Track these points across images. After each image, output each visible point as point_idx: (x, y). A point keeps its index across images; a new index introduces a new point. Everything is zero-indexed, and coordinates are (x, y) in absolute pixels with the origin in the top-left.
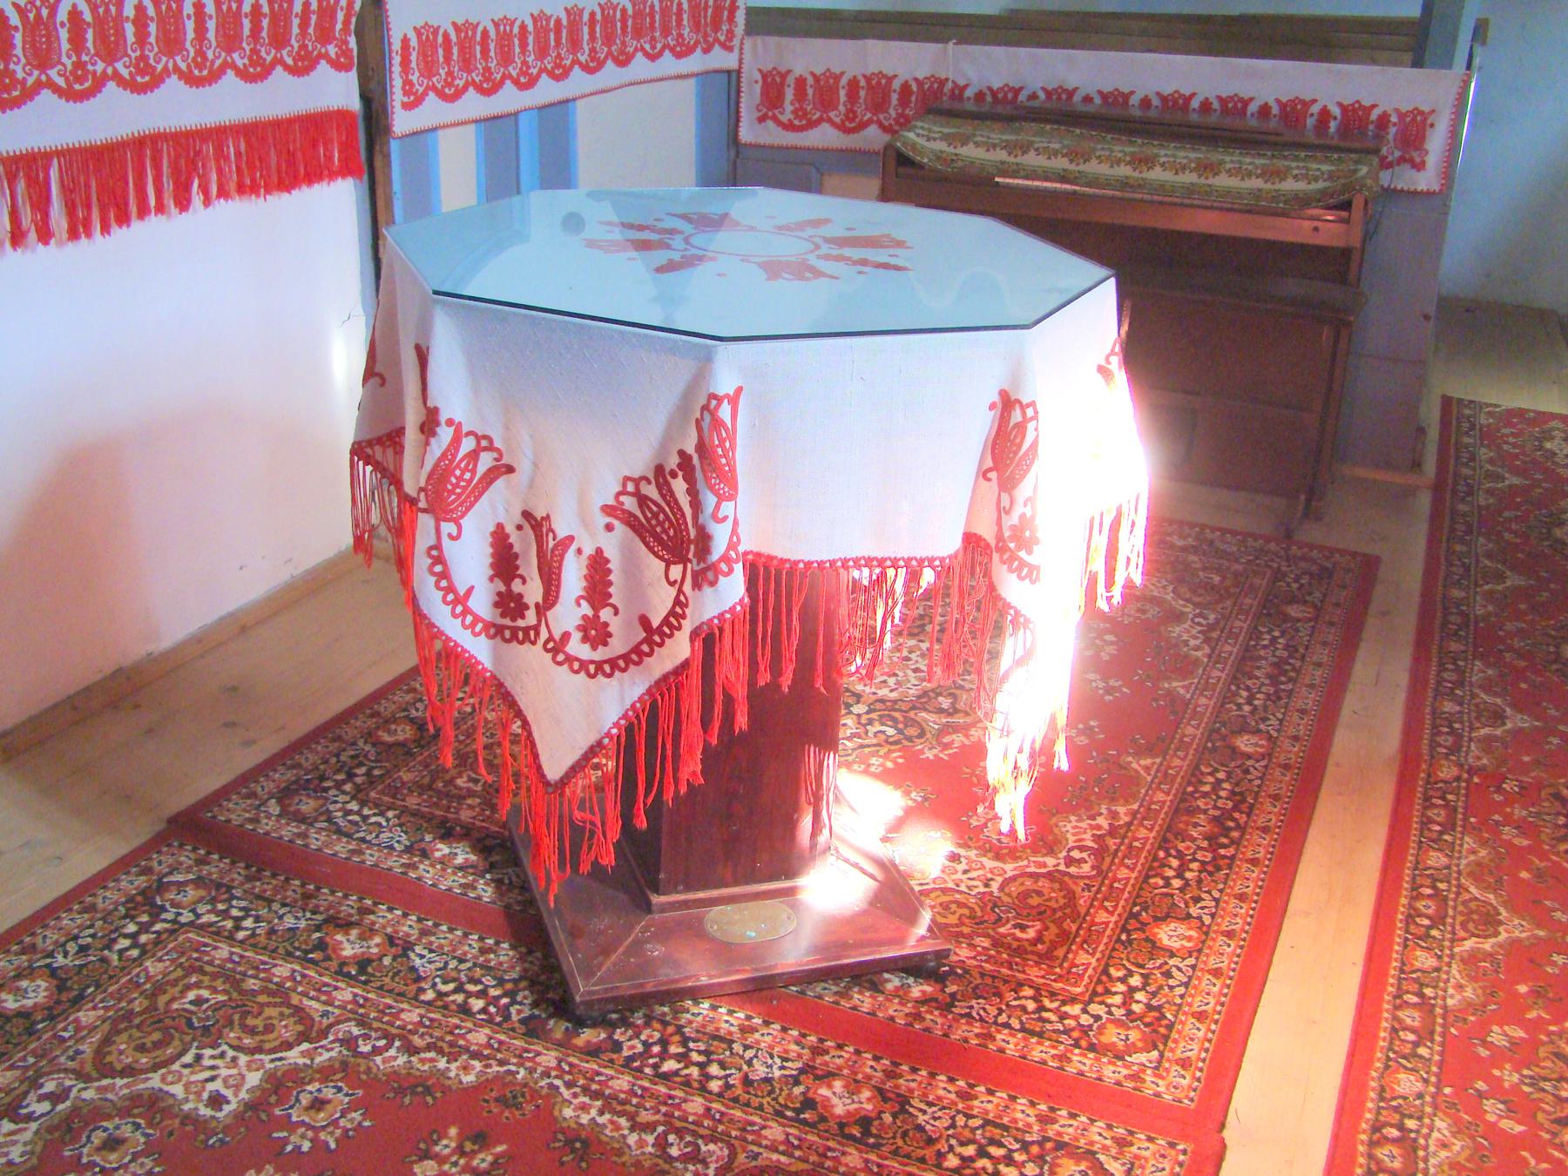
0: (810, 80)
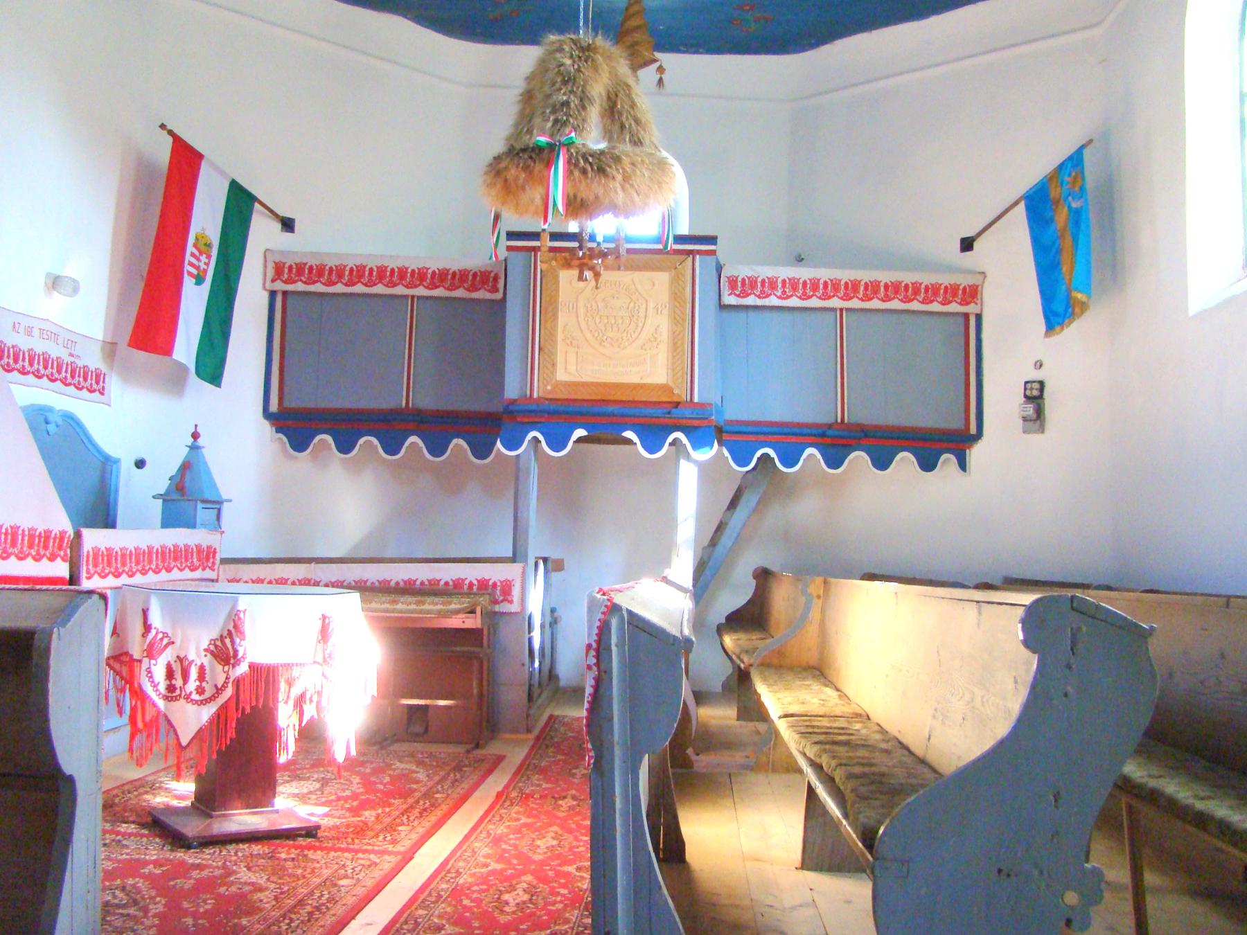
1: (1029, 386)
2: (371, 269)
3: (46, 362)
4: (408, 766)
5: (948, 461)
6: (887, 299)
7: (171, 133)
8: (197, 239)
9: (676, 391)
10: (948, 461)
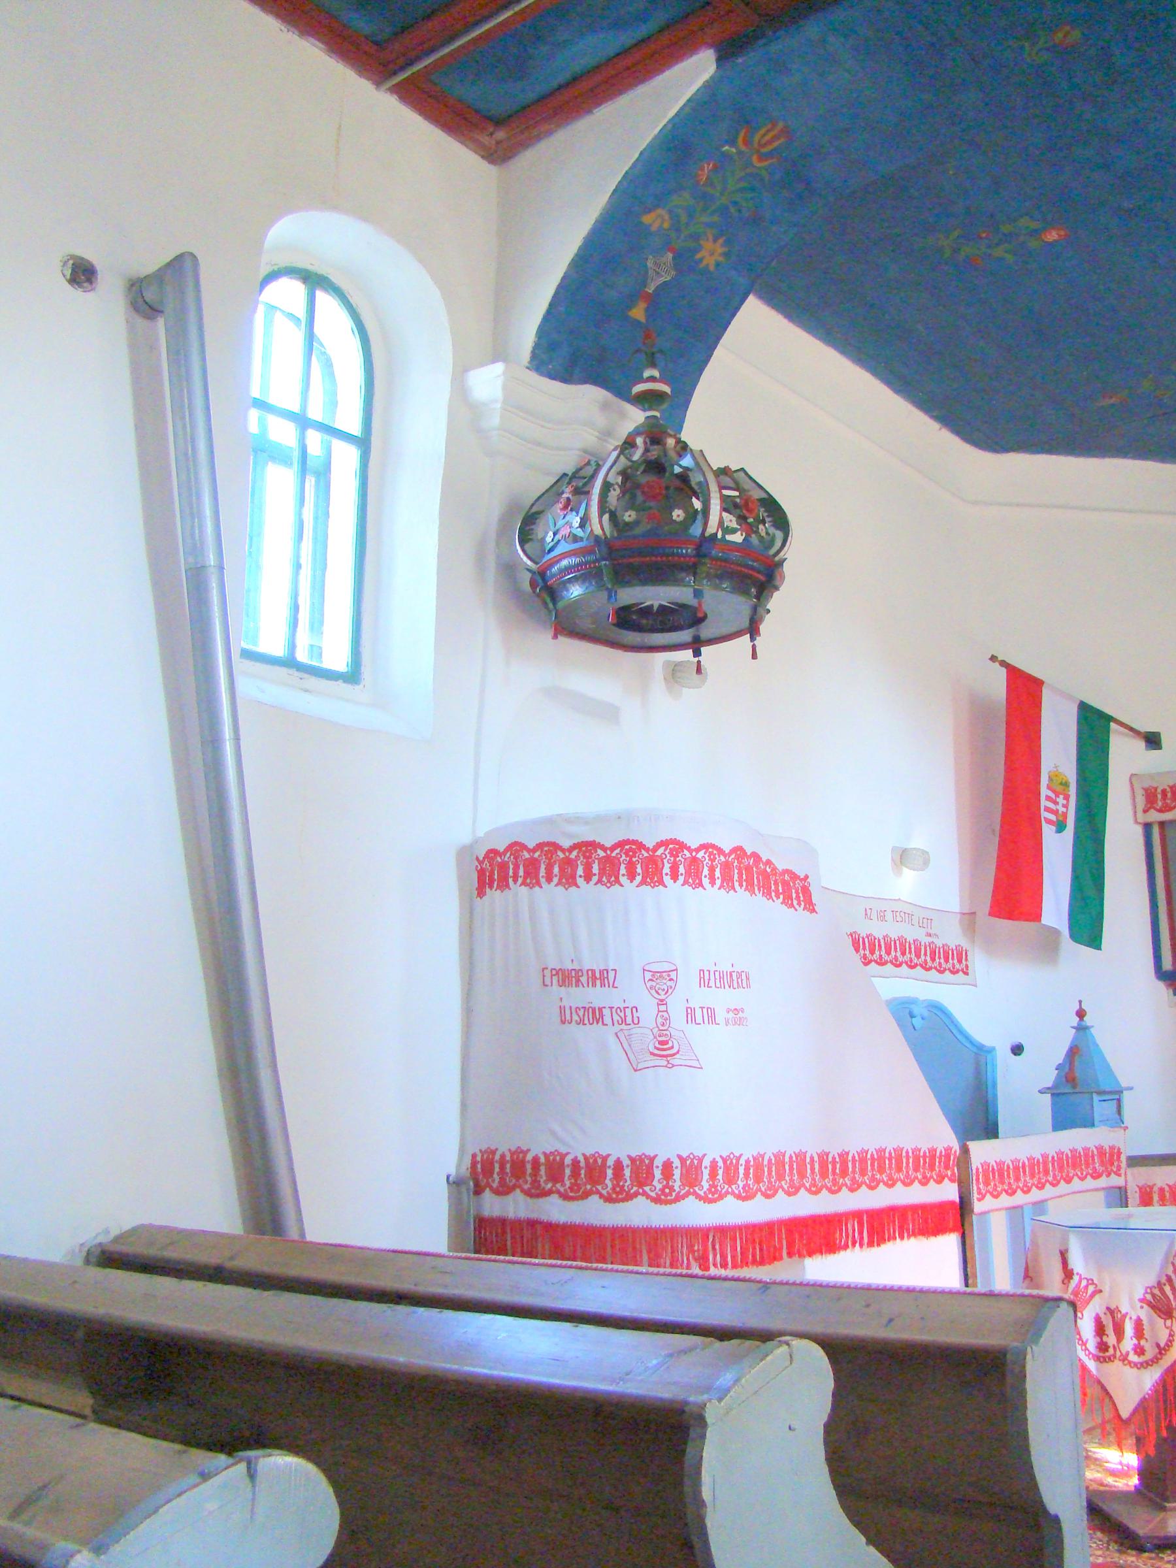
0: (1167, 1189)
3: (903, 946)
7: (1003, 663)
8: (1050, 779)
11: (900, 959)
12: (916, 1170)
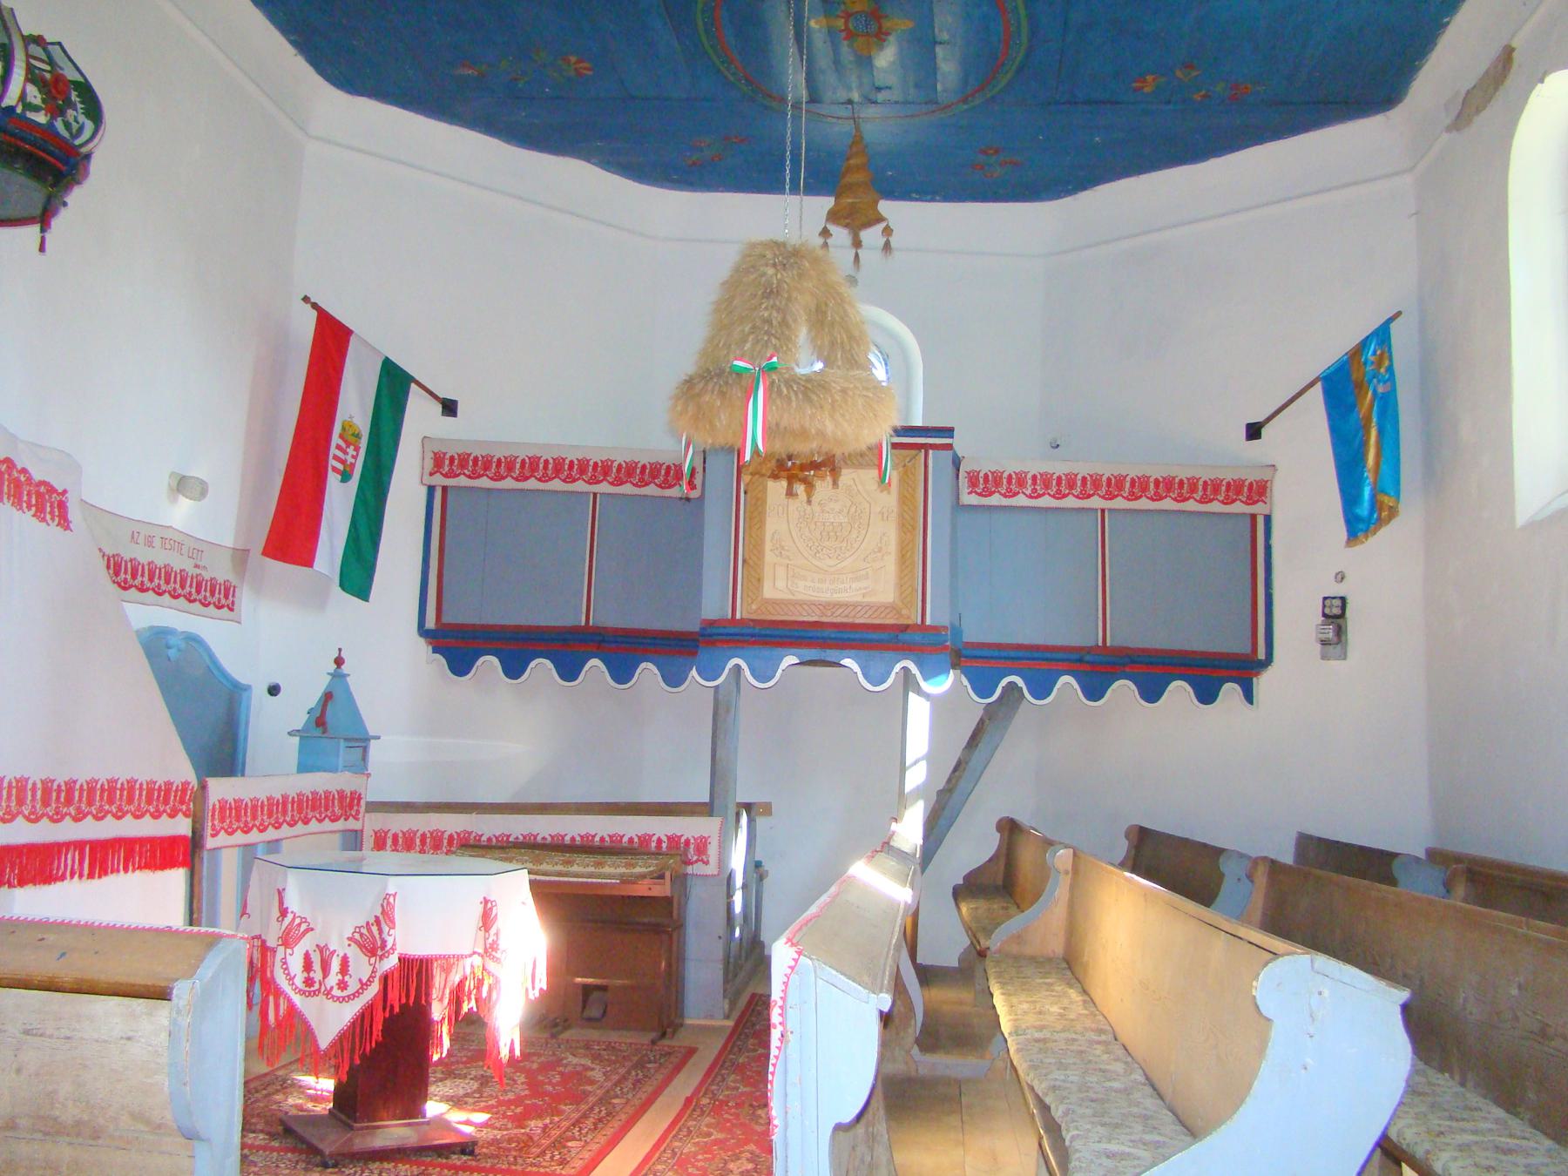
1: (1328, 602)
2: (546, 462)
3: (168, 575)
4: (583, 1061)
5: (1231, 690)
6: (1157, 497)
7: (315, 306)
8: (344, 429)
9: (904, 612)
10: (1231, 690)
11: (164, 587)
12: (149, 802)
